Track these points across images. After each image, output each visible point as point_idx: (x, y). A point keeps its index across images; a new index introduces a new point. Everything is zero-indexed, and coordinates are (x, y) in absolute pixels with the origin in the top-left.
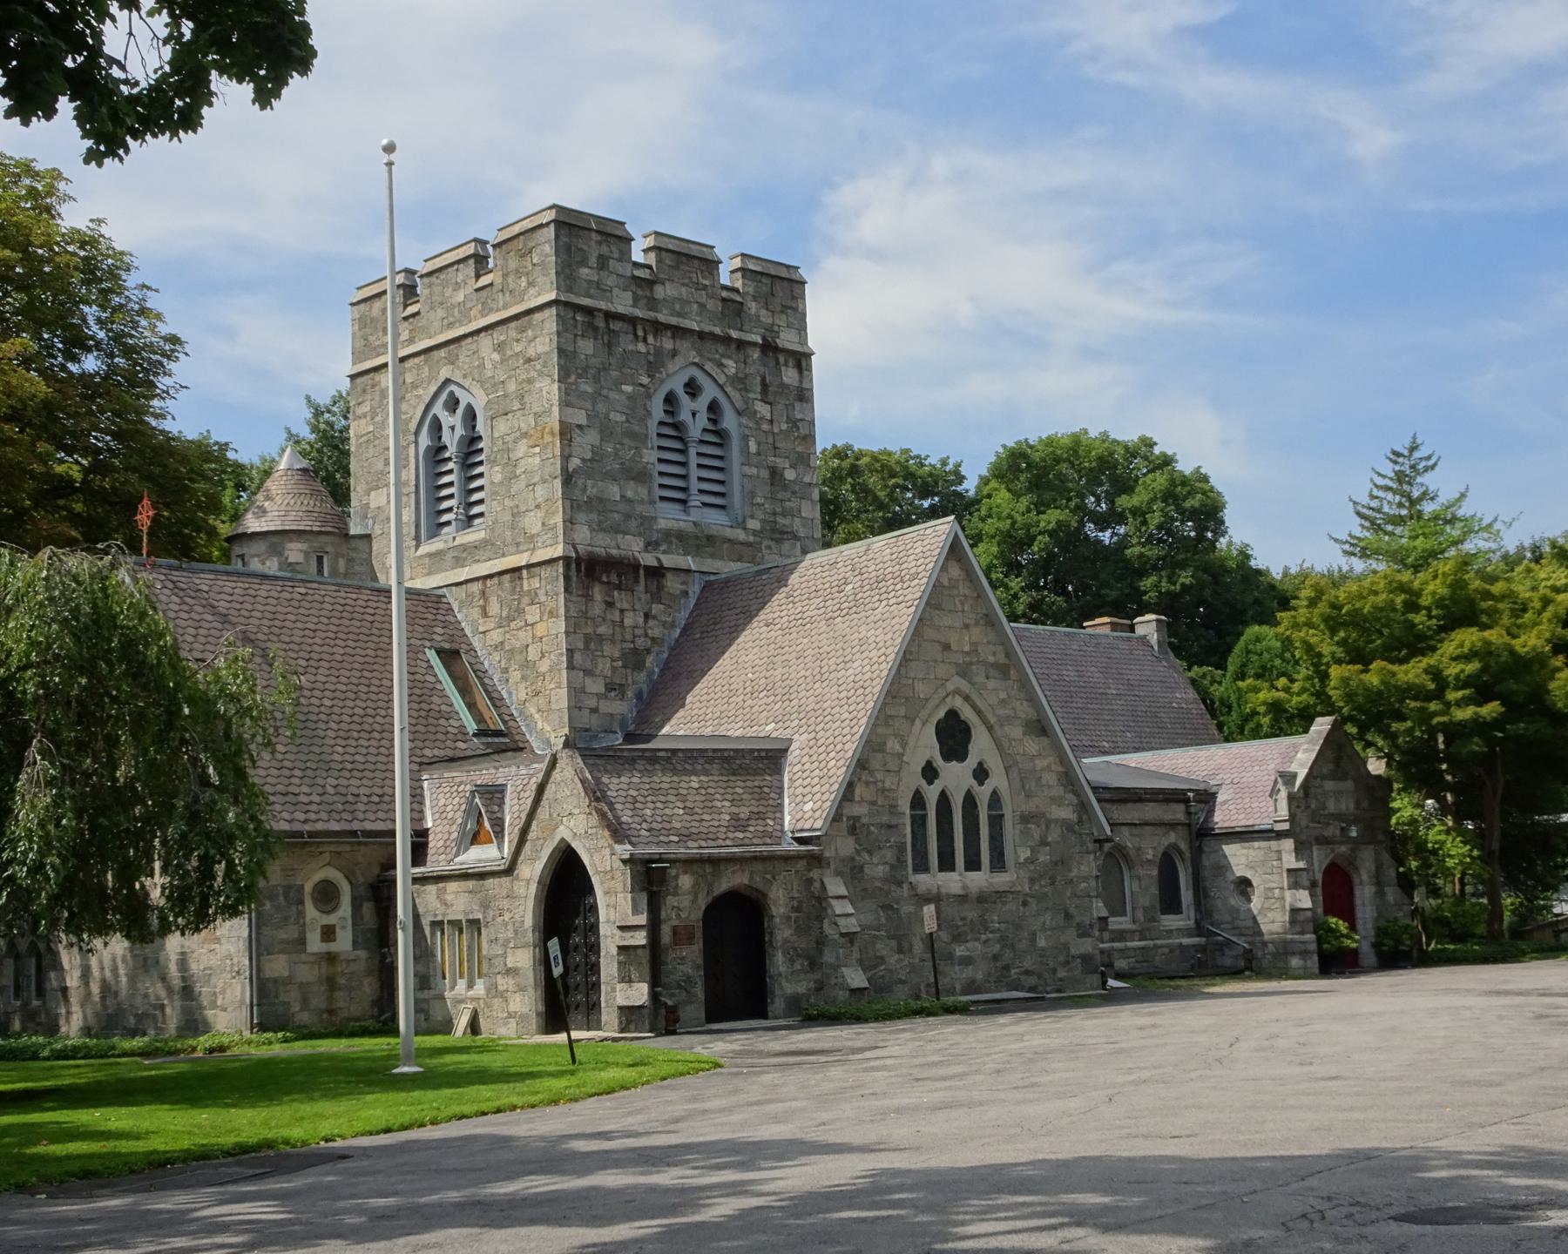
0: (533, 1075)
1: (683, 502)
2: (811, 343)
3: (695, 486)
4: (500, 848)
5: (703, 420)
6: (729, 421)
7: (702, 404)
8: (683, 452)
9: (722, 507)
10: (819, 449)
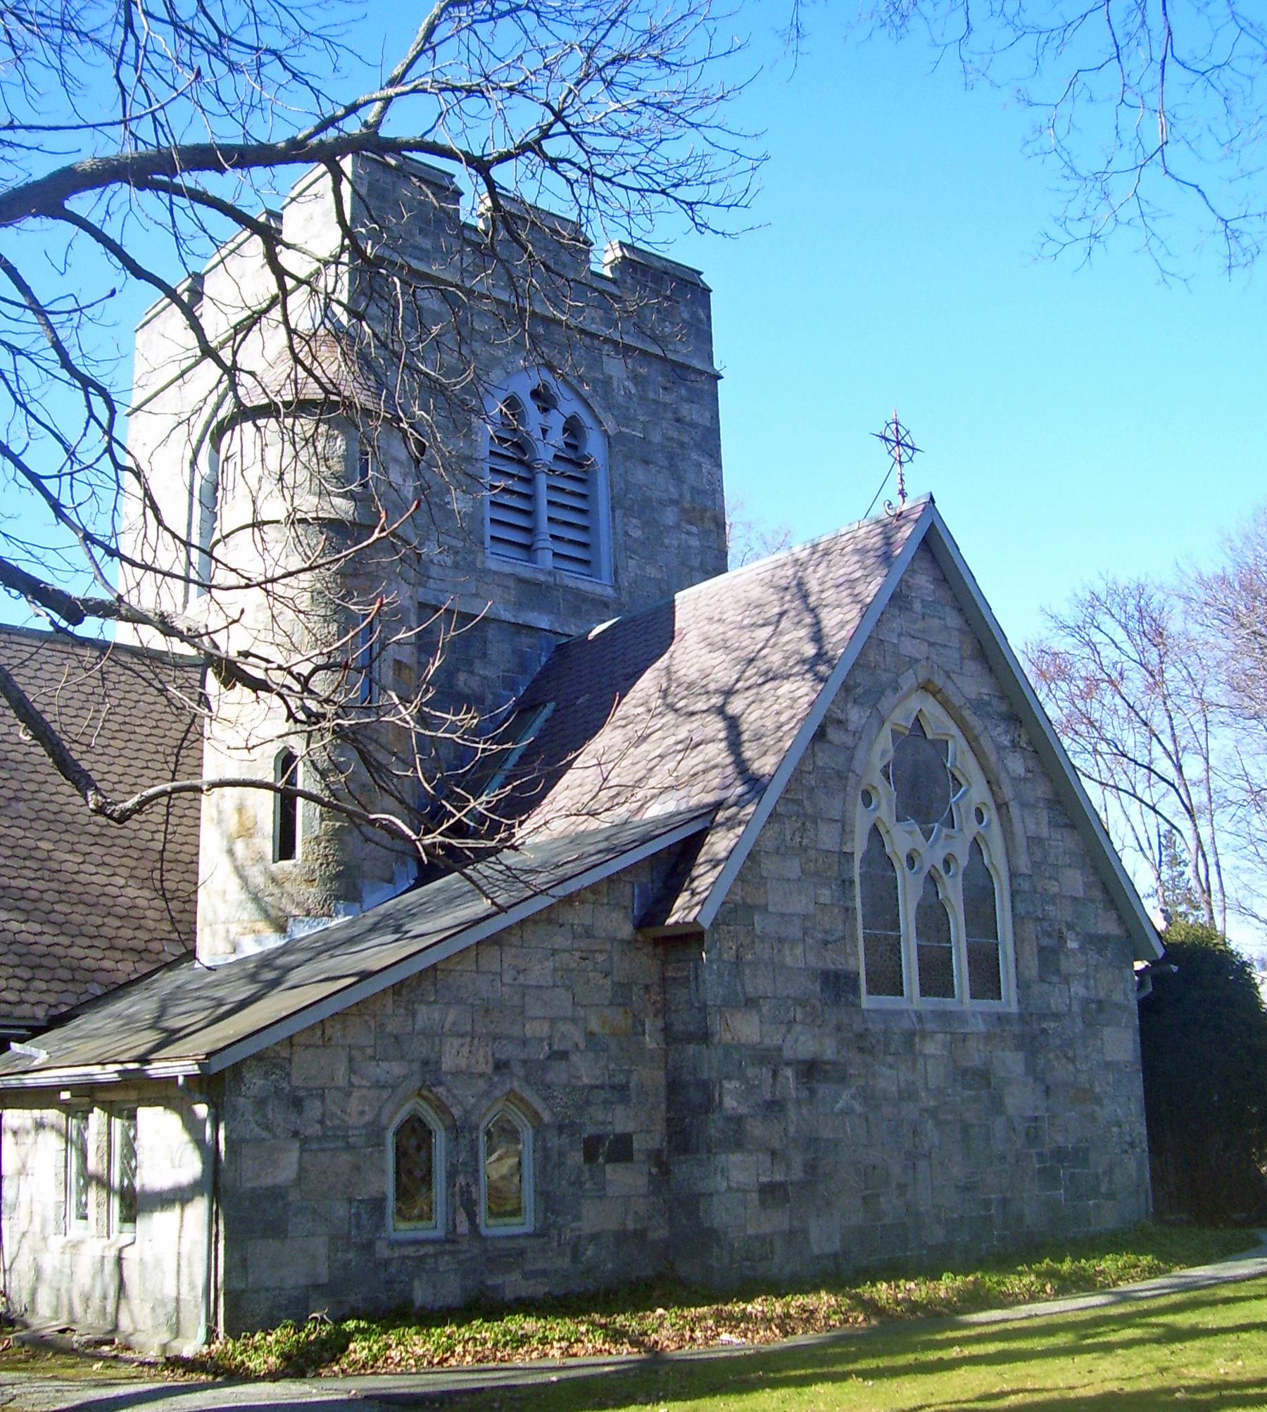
0: (129, 453)
1: (527, 548)
2: (717, 366)
3: (545, 528)
4: (423, 846)
5: (558, 438)
6: (594, 447)
7: (556, 421)
8: (528, 481)
9: (585, 562)
10: (283, 942)
